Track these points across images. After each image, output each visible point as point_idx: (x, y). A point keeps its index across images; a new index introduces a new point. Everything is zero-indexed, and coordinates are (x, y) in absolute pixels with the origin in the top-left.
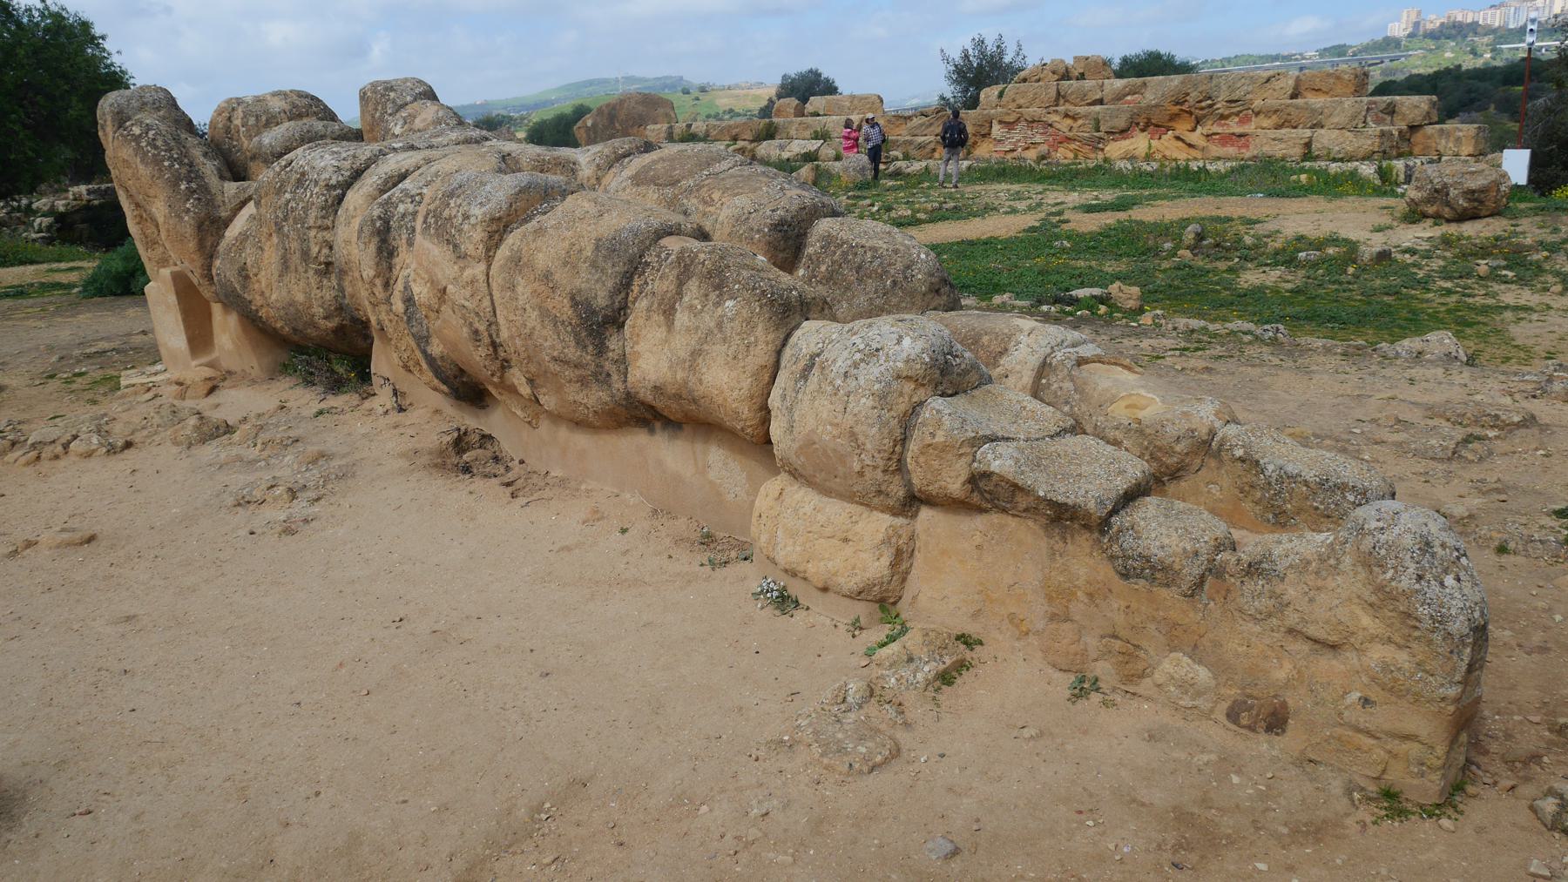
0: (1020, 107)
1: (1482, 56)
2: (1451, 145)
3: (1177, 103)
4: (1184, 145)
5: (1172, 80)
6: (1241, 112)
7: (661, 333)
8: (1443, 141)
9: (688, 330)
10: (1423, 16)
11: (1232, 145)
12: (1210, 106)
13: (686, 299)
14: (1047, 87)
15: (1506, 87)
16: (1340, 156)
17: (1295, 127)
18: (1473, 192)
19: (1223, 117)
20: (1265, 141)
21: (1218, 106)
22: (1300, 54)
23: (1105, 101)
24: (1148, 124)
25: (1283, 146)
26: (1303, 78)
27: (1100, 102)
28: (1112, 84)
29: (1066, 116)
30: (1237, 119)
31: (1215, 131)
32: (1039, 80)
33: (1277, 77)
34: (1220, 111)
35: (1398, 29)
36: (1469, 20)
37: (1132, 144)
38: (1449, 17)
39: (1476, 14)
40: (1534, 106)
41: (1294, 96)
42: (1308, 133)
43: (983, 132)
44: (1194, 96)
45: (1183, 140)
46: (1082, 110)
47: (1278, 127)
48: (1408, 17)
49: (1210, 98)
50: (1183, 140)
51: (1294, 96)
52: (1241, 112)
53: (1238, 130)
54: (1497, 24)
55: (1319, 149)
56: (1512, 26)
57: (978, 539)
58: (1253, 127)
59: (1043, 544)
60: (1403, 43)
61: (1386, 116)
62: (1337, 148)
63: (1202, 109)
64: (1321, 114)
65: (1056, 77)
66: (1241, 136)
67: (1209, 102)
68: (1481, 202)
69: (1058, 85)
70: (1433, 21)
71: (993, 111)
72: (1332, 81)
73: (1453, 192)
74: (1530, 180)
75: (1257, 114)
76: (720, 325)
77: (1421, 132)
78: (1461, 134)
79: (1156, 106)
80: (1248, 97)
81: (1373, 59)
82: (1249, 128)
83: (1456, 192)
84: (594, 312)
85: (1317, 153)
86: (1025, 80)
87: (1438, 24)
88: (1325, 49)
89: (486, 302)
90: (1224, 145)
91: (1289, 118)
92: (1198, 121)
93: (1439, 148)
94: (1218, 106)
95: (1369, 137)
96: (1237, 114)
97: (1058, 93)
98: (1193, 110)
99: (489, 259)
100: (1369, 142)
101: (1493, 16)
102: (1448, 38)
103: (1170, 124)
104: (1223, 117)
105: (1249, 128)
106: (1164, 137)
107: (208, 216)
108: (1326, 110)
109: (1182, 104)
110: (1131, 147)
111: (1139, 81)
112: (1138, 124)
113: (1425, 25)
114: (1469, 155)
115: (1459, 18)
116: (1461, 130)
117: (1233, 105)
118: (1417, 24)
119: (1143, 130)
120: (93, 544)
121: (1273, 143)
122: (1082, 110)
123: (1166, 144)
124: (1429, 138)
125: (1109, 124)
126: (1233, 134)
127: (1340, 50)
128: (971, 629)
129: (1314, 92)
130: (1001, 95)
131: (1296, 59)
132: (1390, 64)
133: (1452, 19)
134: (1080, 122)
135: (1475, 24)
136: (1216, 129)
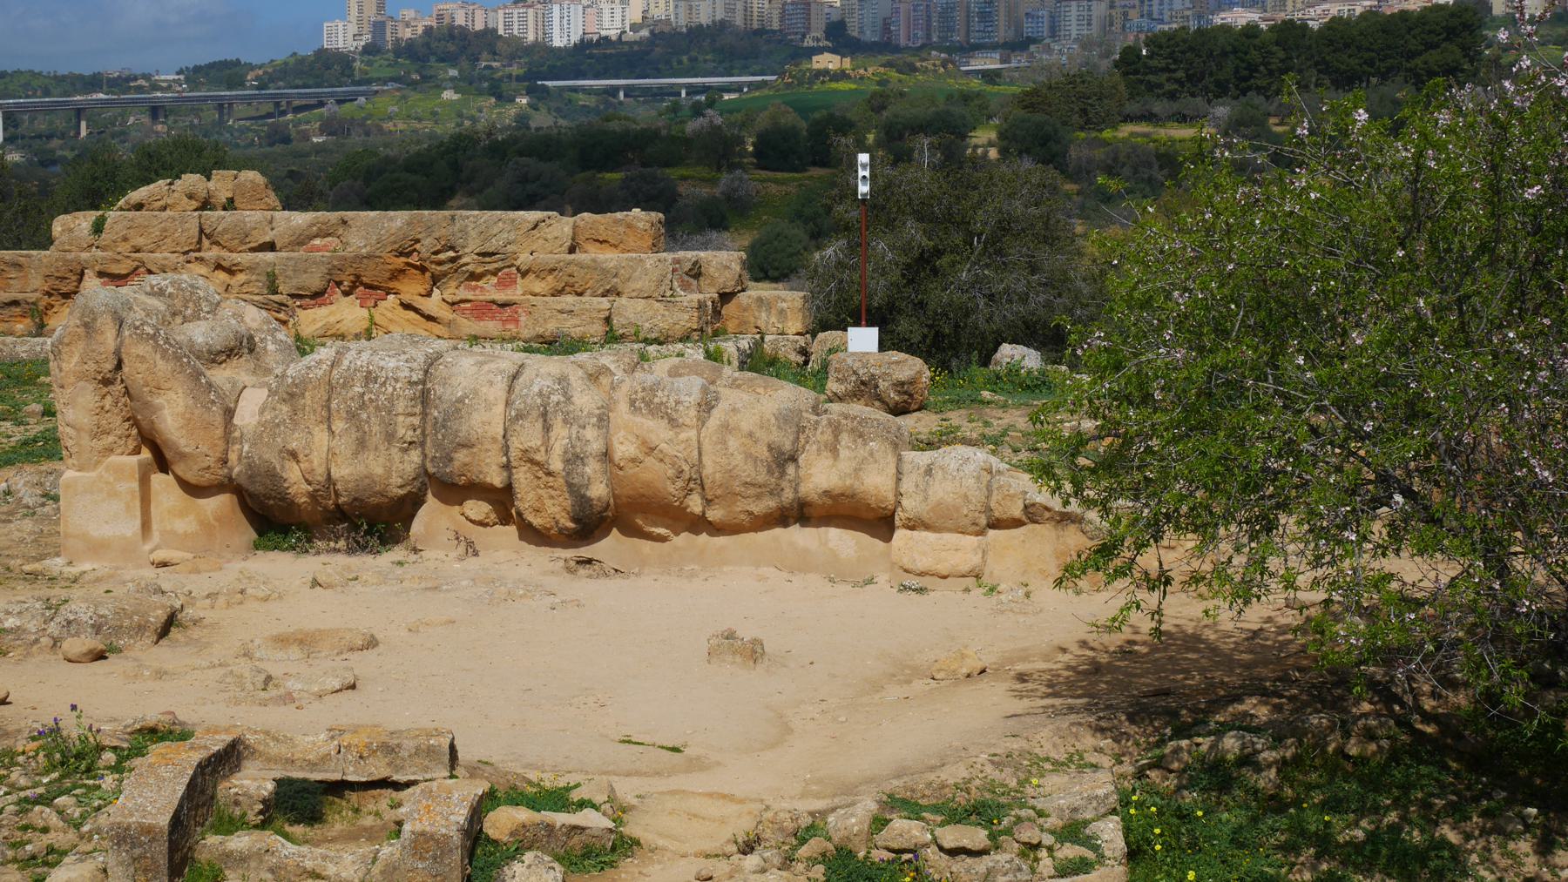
0: (138, 251)
1: (512, 100)
2: (773, 319)
3: (401, 254)
4: (418, 317)
5: (391, 219)
6: (500, 270)
7: (830, 462)
8: (764, 315)
9: (849, 459)
10: (389, 11)
11: (493, 318)
12: (453, 260)
13: (843, 443)
14: (184, 221)
15: (588, 174)
16: (654, 336)
17: (580, 294)
18: (902, 384)
19: (474, 277)
20: (548, 314)
22: (146, 77)
23: (278, 246)
24: (357, 282)
25: (576, 321)
26: (582, 224)
27: (270, 247)
28: (288, 219)
29: (219, 267)
30: (494, 280)
31: (464, 297)
32: (164, 208)
33: (548, 221)
34: (470, 268)
35: (343, 35)
36: (479, 26)
37: (331, 313)
38: (440, 17)
39: (491, 14)
40: (822, 258)
41: (572, 250)
42: (604, 303)
43: (65, 290)
44: (426, 246)
45: (416, 310)
46: (245, 258)
47: (557, 293)
48: (360, 11)
49: (452, 248)
50: (416, 310)
51: (572, 250)
52: (500, 270)
53: (501, 296)
54: (531, 37)
55: (623, 326)
56: (558, 42)
57: (1022, 538)
58: (519, 292)
59: (1053, 534)
60: (357, 64)
61: (691, 280)
62: (647, 325)
63: (440, 263)
64: (616, 276)
65: (195, 204)
66: (504, 305)
67: (451, 254)
68: (911, 396)
69: (200, 216)
70: (411, 23)
71: (84, 255)
72: (621, 229)
73: (883, 385)
75: (524, 274)
76: (871, 454)
77: (734, 301)
78: (785, 305)
79: (368, 257)
80: (510, 248)
81: (301, 96)
82: (515, 293)
83: (886, 384)
84: (784, 454)
85: (621, 331)
86: (139, 207)
87: (420, 31)
88: (197, 69)
89: (696, 453)
90: (479, 318)
91: (571, 280)
92: (435, 280)
93: (761, 324)
95: (683, 310)
96: (495, 273)
97: (201, 231)
98: (427, 264)
99: (702, 422)
100: (686, 317)
101: (523, 19)
102: (442, 60)
103: (391, 285)
104: (474, 277)
105: (515, 293)
106: (382, 304)
108: (622, 271)
109: (408, 255)
110: (332, 319)
111: (334, 216)
112: (339, 284)
113: (395, 28)
114: (798, 334)
115: (460, 21)
116: (784, 300)
117: (488, 259)
118: (378, 28)
119: (346, 294)
121: (561, 316)
122: (245, 258)
123: (389, 315)
124: (745, 310)
125: (294, 282)
126: (493, 302)
127: (227, 73)
128: (1024, 580)
129: (598, 244)
130: (98, 228)
131: (140, 89)
132: (336, 108)
133: (446, 21)
134: (241, 277)
135: (489, 34)
136: (463, 293)
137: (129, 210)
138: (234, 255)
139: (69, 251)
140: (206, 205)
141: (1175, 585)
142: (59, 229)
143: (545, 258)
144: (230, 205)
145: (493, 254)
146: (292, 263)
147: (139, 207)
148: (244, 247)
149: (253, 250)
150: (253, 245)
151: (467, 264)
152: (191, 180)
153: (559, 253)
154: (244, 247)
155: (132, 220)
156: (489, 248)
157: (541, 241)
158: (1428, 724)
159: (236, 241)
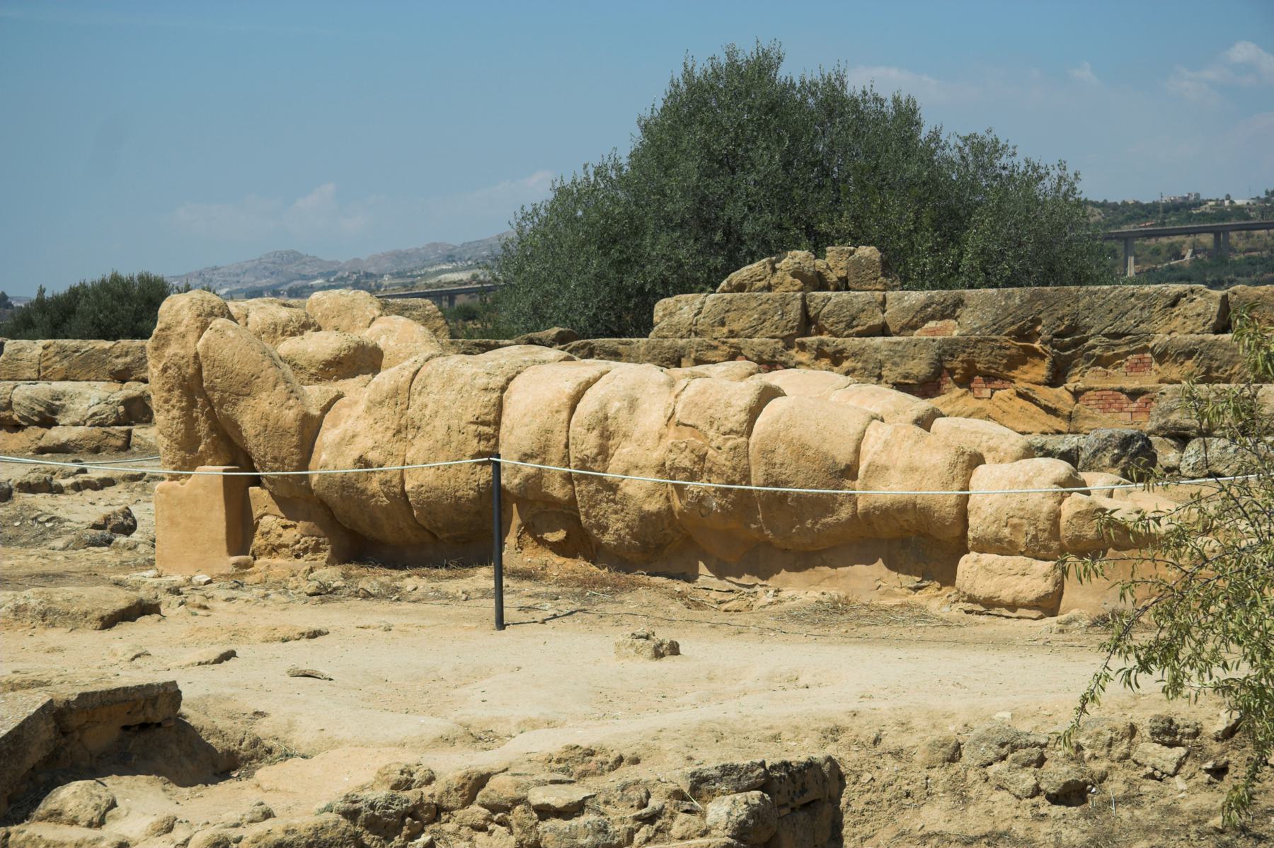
12: (1076, 344)
21: (1091, 342)
23: (892, 329)
27: (883, 330)
34: (1097, 351)
46: (854, 343)
53: (1132, 384)
69: (804, 298)
74: (483, 563)
86: (740, 288)
94: (1091, 342)
107: (1148, 451)
117: (1117, 341)
120: (232, 661)
126: (1121, 390)
137: (731, 291)
138: (840, 340)
139: (666, 337)
140: (819, 283)
141: (624, 763)
142: (661, 314)
143: (1183, 338)
144: (843, 285)
145: (1124, 335)
146: (900, 348)
147: (740, 288)
148: (851, 331)
149: (859, 334)
150: (859, 328)
151: (1094, 347)
152: (798, 257)
153: (1203, 332)
154: (851, 331)
155: (730, 302)
156: (1119, 327)
157: (1180, 319)
158: (402, 831)
159: (842, 325)
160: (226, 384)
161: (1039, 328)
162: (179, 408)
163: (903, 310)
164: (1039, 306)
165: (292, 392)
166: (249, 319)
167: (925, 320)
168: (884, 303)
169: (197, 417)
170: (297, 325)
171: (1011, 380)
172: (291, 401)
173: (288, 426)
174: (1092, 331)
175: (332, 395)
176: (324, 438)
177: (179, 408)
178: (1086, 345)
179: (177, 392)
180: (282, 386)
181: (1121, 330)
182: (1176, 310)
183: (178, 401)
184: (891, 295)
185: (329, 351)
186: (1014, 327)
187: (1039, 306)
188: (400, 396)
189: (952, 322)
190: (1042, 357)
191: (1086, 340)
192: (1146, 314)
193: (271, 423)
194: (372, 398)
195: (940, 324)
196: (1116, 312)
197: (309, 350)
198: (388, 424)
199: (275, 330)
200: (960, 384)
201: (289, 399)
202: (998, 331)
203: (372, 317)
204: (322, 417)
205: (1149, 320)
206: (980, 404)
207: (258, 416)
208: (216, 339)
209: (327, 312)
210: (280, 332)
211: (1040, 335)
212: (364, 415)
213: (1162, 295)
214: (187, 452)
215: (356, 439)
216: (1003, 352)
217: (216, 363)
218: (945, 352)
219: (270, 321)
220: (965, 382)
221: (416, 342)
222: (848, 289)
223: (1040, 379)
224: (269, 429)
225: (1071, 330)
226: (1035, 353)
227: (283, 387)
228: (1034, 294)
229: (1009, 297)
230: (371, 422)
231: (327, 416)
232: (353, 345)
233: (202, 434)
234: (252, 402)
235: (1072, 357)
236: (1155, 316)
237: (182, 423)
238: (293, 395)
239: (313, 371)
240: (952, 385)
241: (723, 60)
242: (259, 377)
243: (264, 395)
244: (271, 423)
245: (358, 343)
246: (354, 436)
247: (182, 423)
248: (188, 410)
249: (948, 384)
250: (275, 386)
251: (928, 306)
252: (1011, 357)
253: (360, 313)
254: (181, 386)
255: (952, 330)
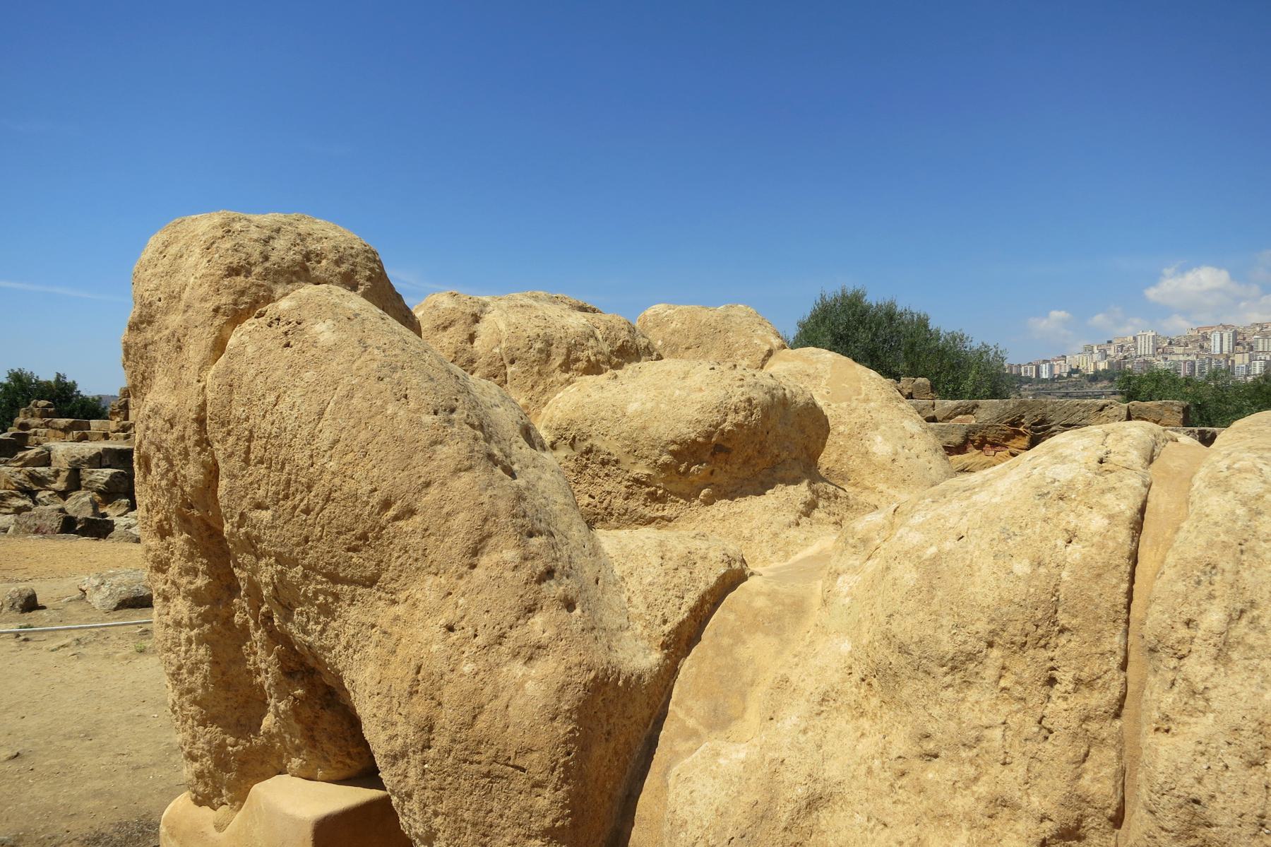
12: (1044, 429)
21: (1053, 428)
94: (1053, 428)
157: (1105, 417)
160: (291, 532)
161: (1023, 421)
162: (189, 594)
163: (944, 409)
164: (1023, 409)
165: (549, 573)
166: (481, 328)
167: (956, 415)
168: (934, 406)
169: (245, 626)
170: (606, 348)
171: (1006, 447)
172: (538, 620)
173: (516, 739)
174: (1054, 423)
175: (708, 577)
176: (677, 795)
177: (189, 594)
178: (1051, 430)
179: (179, 540)
180: (504, 553)
181: (1071, 423)
182: (1103, 413)
183: (186, 571)
184: (937, 402)
185: (692, 412)
186: (1009, 420)
187: (1023, 409)
188: (1069, 645)
189: (971, 416)
190: (1024, 435)
191: (1050, 427)
192: (1086, 415)
193: (447, 717)
194: (906, 628)
195: (964, 417)
196: (1068, 413)
197: (632, 408)
198: (1010, 780)
199: (546, 354)
200: (977, 448)
201: (531, 610)
202: (1000, 421)
203: (767, 348)
204: (669, 673)
205: (1087, 418)
206: (989, 458)
207: (400, 675)
208: (262, 352)
209: (675, 339)
210: (557, 360)
211: (1023, 424)
212: (853, 692)
213: (1095, 404)
214: (227, 728)
215: (824, 817)
216: (1003, 432)
217: (257, 452)
218: (970, 431)
219: (532, 332)
220: (980, 447)
221: (867, 400)
222: (912, 398)
223: (1023, 447)
224: (441, 741)
225: (1042, 422)
226: (1020, 433)
227: (510, 555)
228: (1021, 403)
229: (1006, 404)
230: (900, 743)
231: (687, 667)
232: (759, 396)
233: (266, 680)
234: (384, 614)
235: (1042, 436)
236: (1091, 416)
237: (201, 640)
238: (553, 589)
239: (641, 470)
240: (973, 448)
241: (840, 294)
242: (410, 512)
243: (427, 589)
244: (447, 717)
245: (770, 391)
246: (813, 803)
247: (201, 640)
248: (216, 601)
249: (970, 447)
250: (475, 552)
251: (958, 408)
252: (1006, 435)
253: (743, 340)
254: (185, 522)
255: (972, 421)
